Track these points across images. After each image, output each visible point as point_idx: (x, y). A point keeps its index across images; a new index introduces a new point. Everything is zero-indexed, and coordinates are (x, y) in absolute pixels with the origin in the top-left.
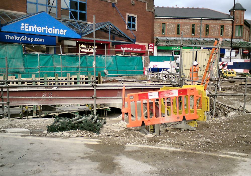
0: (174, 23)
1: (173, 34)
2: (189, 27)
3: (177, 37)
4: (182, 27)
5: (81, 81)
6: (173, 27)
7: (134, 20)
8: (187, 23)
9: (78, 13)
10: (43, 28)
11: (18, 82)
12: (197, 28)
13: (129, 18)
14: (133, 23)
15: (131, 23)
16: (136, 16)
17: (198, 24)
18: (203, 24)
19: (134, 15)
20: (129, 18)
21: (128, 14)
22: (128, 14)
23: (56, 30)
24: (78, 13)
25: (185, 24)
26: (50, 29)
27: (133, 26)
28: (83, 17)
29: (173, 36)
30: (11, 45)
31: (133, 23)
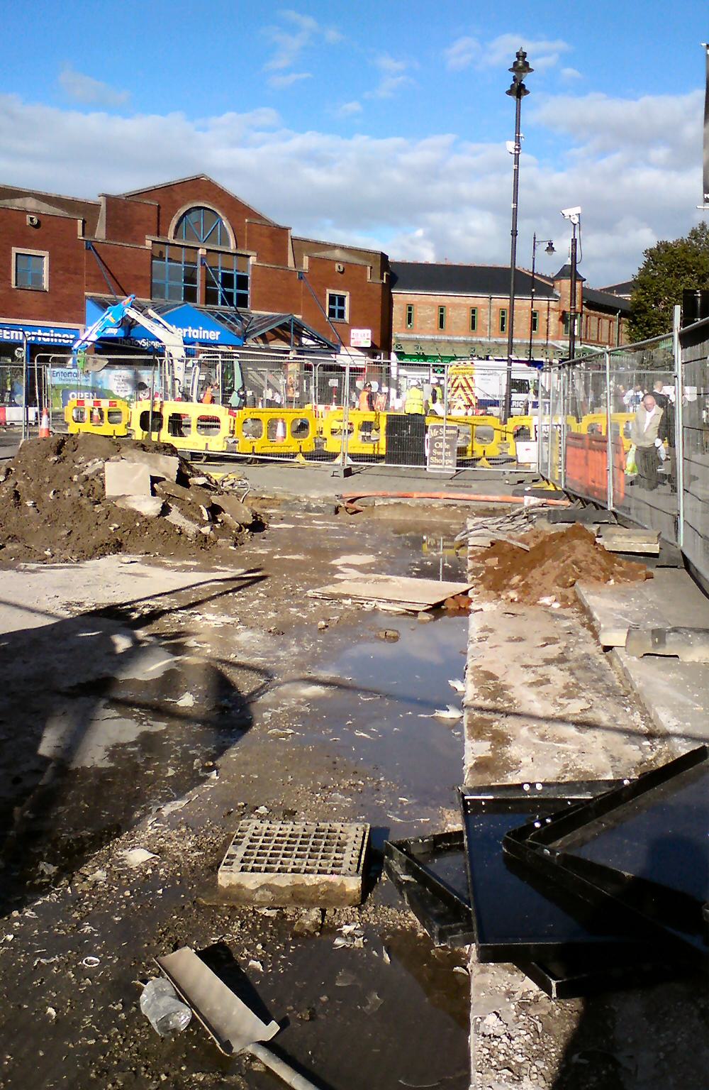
0: (432, 304)
1: (431, 329)
2: (465, 315)
3: (440, 334)
4: (449, 314)
5: (540, 400)
6: (429, 313)
7: (342, 302)
8: (459, 306)
9: (235, 287)
10: (185, 330)
11: (513, 377)
12: (483, 318)
13: (332, 298)
14: (341, 308)
15: (337, 307)
16: (347, 294)
17: (483, 306)
18: (496, 307)
19: (342, 293)
20: (332, 298)
21: (329, 291)
22: (329, 291)
23: (204, 332)
24: (235, 287)
25: (455, 306)
26: (195, 331)
27: (341, 314)
28: (243, 301)
29: (431, 332)
30: (100, 605)
31: (341, 308)
